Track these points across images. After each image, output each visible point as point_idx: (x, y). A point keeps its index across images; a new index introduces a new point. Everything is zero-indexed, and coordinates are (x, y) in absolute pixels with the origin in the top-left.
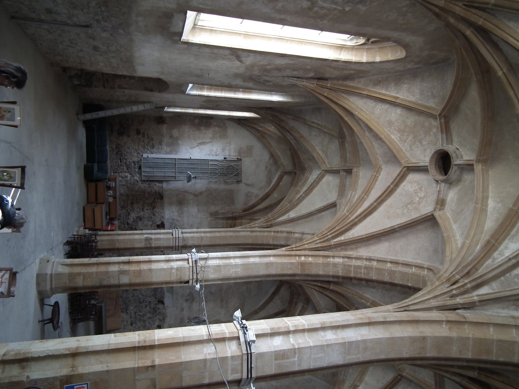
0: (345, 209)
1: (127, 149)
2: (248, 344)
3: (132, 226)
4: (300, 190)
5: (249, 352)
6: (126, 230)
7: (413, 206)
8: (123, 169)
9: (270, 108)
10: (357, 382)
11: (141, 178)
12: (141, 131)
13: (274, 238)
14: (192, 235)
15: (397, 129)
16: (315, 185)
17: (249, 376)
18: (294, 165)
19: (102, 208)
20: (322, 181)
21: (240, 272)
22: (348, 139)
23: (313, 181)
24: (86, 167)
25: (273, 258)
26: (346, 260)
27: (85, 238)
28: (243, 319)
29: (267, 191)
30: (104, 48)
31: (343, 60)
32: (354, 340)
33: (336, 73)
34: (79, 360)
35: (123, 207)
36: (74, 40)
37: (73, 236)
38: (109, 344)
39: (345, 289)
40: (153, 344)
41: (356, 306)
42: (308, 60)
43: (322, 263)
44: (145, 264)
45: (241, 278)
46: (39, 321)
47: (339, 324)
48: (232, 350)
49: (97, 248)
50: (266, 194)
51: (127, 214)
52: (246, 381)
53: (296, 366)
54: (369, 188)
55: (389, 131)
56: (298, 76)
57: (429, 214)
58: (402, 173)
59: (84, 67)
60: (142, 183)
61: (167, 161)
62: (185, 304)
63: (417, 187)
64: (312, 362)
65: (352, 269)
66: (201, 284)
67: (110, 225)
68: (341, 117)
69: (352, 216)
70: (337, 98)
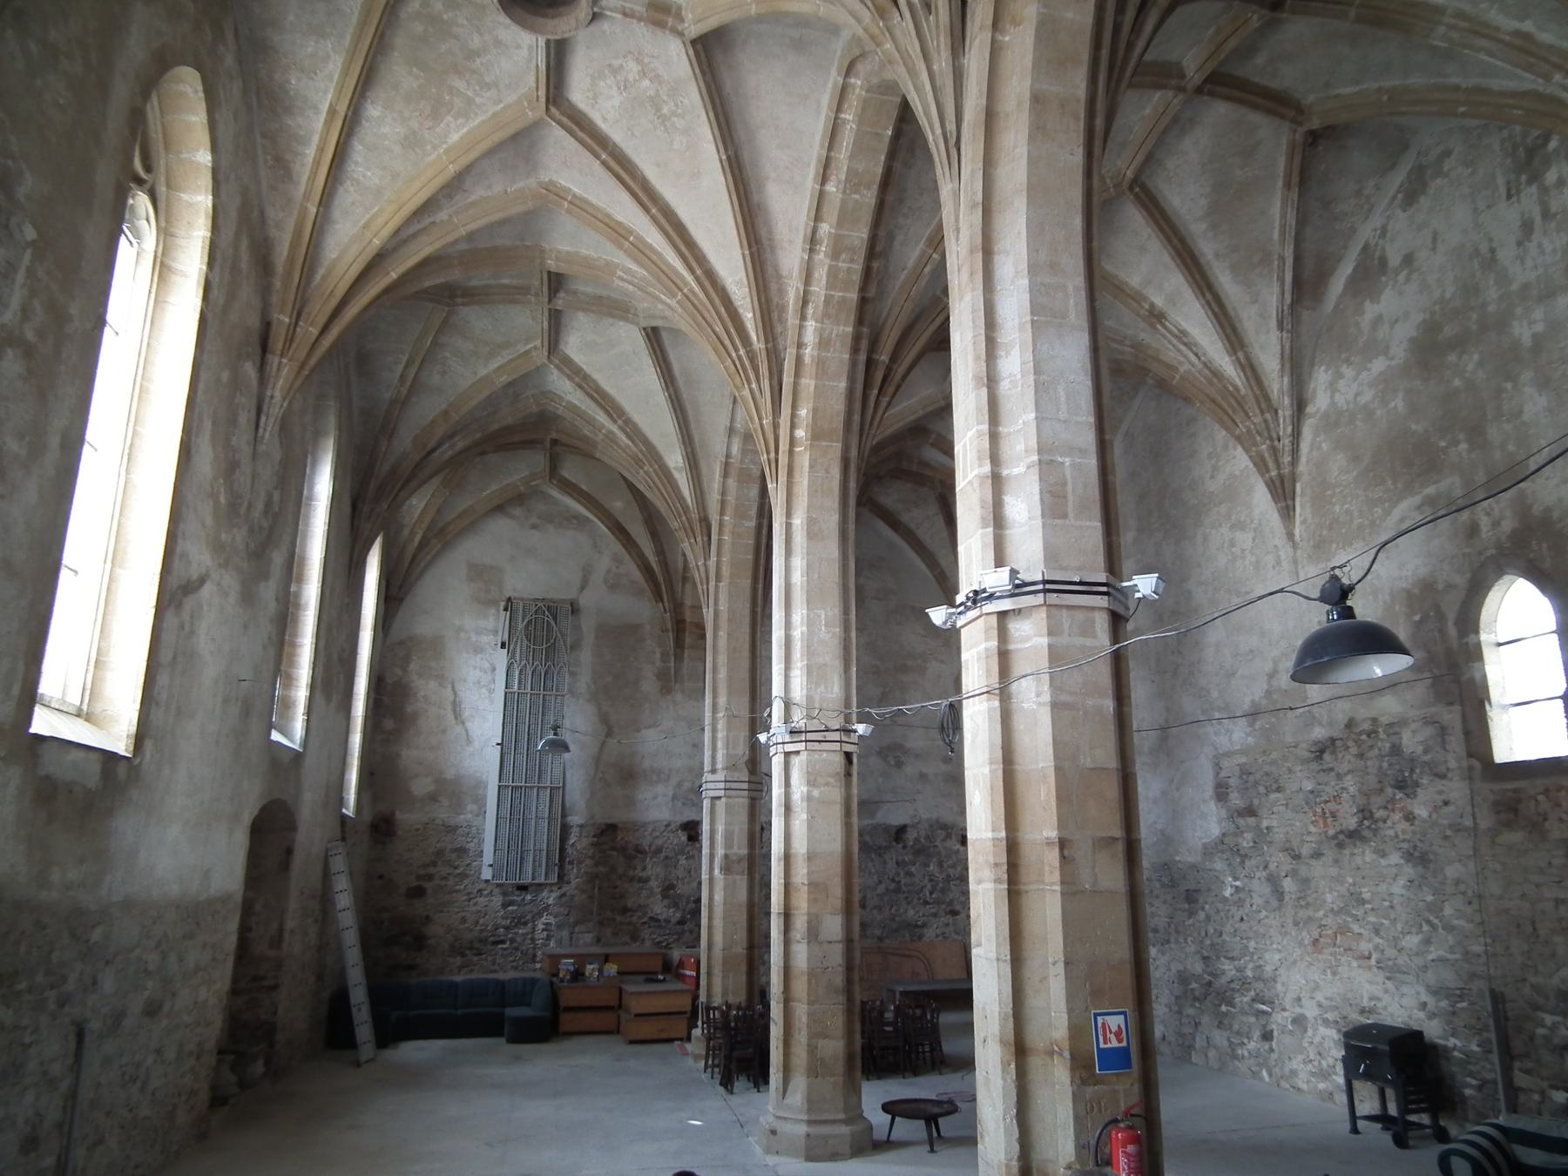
0: (664, 303)
1: (466, 925)
2: (1019, 588)
3: (687, 910)
4: (604, 431)
5: (1040, 587)
6: (699, 926)
7: (665, 98)
8: (523, 934)
9: (354, 507)
10: (1142, 307)
11: (552, 885)
12: (415, 884)
13: (740, 514)
14: (720, 745)
15: (431, 124)
16: (592, 385)
17: (1104, 589)
18: (530, 444)
19: (632, 994)
20: (580, 364)
21: (830, 613)
22: (455, 275)
23: (579, 393)
24: (513, 1040)
25: (794, 516)
26: (810, 311)
27: (715, 1037)
28: (952, 604)
29: (606, 530)
30: (150, 984)
31: (205, 268)
32: (1027, 296)
33: (247, 294)
34: (1036, 1037)
35: (635, 937)
36: (123, 1074)
37: (709, 1070)
38: (998, 960)
39: (890, 323)
40: (1004, 842)
41: (938, 292)
42: (204, 376)
43: (817, 378)
44: (793, 872)
45: (846, 612)
46: (932, 1151)
47: (983, 338)
48: (1032, 632)
49: (743, 1005)
50: (613, 533)
51: (652, 924)
52: (1116, 599)
53: (1087, 461)
54: (606, 224)
55: (435, 147)
56: (254, 412)
57: (691, 52)
58: (565, 120)
59: (211, 1044)
60: (569, 882)
61: (506, 812)
62: (910, 769)
63: (610, 80)
64: (1079, 419)
65: (838, 294)
66: (854, 717)
67: (682, 971)
68: (387, 290)
69: (686, 284)
70: (328, 297)
